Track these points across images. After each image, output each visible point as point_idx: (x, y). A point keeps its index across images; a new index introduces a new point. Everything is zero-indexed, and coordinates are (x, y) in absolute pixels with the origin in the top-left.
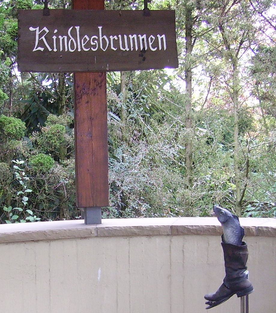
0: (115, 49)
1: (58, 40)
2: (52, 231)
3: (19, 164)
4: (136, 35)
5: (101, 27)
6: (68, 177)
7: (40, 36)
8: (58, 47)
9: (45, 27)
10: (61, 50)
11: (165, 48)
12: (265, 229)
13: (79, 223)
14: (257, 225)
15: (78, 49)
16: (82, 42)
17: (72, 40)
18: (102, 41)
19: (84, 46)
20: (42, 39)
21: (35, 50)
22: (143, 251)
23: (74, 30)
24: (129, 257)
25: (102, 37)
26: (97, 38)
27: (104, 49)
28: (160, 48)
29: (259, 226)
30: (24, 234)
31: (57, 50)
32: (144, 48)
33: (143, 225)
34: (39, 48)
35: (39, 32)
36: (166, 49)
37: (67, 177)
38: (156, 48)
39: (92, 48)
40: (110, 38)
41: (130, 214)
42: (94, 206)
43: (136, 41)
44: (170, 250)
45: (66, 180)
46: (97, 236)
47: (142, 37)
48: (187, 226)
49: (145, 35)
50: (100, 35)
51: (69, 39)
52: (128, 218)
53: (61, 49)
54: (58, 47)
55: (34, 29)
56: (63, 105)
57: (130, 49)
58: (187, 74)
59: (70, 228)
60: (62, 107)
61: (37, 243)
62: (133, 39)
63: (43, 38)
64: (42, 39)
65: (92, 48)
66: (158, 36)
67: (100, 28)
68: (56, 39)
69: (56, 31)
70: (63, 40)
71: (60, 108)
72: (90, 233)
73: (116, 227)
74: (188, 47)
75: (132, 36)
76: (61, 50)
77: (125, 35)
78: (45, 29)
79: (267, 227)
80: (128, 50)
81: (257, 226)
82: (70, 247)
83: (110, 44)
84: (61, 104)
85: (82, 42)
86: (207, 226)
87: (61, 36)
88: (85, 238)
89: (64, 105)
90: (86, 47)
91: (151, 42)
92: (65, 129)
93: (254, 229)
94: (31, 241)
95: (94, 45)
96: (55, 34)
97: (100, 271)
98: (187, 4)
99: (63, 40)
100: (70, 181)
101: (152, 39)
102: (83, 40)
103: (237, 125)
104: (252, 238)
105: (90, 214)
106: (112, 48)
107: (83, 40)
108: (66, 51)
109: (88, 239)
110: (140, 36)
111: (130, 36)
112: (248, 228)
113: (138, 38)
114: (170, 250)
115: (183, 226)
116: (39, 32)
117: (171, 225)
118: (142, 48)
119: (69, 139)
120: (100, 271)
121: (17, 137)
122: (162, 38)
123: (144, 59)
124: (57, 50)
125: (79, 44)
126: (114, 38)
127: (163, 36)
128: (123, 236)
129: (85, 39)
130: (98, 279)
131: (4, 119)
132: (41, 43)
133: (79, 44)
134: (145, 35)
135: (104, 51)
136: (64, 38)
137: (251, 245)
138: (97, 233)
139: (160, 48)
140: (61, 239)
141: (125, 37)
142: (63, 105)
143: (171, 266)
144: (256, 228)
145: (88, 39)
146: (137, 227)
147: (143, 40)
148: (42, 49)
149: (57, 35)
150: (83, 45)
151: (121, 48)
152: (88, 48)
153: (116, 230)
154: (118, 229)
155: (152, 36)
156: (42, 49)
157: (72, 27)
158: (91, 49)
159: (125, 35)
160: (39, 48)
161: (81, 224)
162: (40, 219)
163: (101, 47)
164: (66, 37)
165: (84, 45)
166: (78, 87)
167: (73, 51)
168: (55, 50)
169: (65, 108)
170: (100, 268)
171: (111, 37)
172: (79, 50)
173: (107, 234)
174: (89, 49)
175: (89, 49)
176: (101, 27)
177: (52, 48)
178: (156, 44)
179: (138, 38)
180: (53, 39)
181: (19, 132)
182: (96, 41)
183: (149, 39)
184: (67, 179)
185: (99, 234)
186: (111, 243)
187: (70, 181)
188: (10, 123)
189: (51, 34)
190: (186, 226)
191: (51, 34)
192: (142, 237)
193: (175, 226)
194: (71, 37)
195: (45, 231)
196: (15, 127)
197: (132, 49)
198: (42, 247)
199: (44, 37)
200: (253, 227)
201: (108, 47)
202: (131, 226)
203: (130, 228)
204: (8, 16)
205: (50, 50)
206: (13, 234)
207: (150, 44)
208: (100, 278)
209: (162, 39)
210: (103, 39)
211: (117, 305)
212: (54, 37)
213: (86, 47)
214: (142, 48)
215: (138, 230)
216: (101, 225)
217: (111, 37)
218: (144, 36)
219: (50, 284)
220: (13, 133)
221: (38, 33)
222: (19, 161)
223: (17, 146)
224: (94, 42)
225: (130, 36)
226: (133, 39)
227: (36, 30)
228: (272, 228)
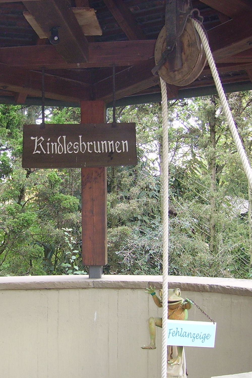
0: (91, 152)
1: (50, 146)
2: (60, 282)
3: (68, 231)
4: (106, 141)
5: (81, 136)
6: (110, 242)
7: (38, 143)
8: (50, 151)
9: (42, 137)
10: (52, 153)
11: (127, 151)
12: (215, 287)
13: (84, 277)
14: (210, 283)
15: (64, 152)
16: (68, 147)
17: (60, 146)
18: (82, 146)
19: (69, 150)
20: (39, 145)
21: (34, 153)
22: (128, 300)
23: (62, 138)
24: (118, 305)
25: (82, 143)
26: (78, 144)
27: (83, 152)
28: (124, 151)
29: (211, 284)
30: (38, 283)
31: (49, 153)
32: (112, 150)
33: (128, 281)
34: (37, 152)
35: (37, 140)
36: (128, 151)
37: (109, 242)
38: (121, 151)
39: (74, 151)
40: (87, 144)
41: (158, 272)
42: (94, 265)
43: (106, 146)
44: (148, 300)
45: (109, 244)
46: (94, 288)
47: (111, 143)
48: (160, 282)
49: (113, 141)
50: (81, 142)
51: (58, 145)
52: (157, 275)
53: (53, 152)
54: (50, 151)
55: (34, 138)
56: (114, 185)
57: (102, 152)
58: (212, 162)
59: (74, 281)
60: (114, 187)
61: (49, 290)
62: (104, 144)
63: (40, 144)
64: (39, 145)
65: (74, 151)
66: (122, 141)
67: (80, 137)
68: (49, 145)
69: (49, 139)
70: (54, 145)
71: (112, 188)
72: (88, 285)
73: (107, 281)
74: (212, 141)
75: (103, 142)
76: (52, 153)
77: (98, 142)
78: (42, 138)
79: (217, 285)
80: (100, 152)
81: (210, 284)
82: (73, 294)
83: (87, 148)
84: (113, 185)
85: (68, 147)
86: (175, 283)
87: (53, 143)
88: (85, 288)
89: (115, 186)
90: (70, 150)
91: (117, 146)
92: (110, 204)
93: (208, 286)
94: (44, 289)
95: (76, 149)
96: (49, 142)
97: (96, 313)
98: (206, 108)
99: (54, 145)
100: (112, 245)
101: (118, 144)
102: (68, 146)
103: (250, 202)
104: (207, 293)
105: (92, 270)
106: (89, 151)
107: (68, 146)
108: (56, 153)
109: (88, 289)
110: (109, 142)
111: (102, 142)
112: (204, 286)
113: (108, 144)
114: (148, 300)
115: (157, 282)
116: (37, 140)
117: (148, 281)
118: (110, 151)
119: (113, 213)
120: (96, 313)
121: (71, 211)
122: (125, 143)
123: (112, 159)
124: (49, 153)
125: (65, 148)
126: (90, 144)
127: (126, 142)
128: (113, 288)
129: (70, 145)
130: (94, 320)
131: (61, 197)
132: (39, 148)
133: (65, 148)
134: (113, 141)
135: (83, 153)
136: (55, 144)
137: (206, 299)
138: (94, 285)
139: (124, 151)
140: (66, 288)
141: (98, 143)
142: (114, 185)
143: (148, 313)
144: (209, 286)
145: (72, 145)
146: (124, 281)
147: (111, 144)
148: (39, 152)
149: (50, 142)
150: (68, 149)
151: (95, 151)
152: (71, 152)
153: (108, 283)
154: (109, 283)
155: (117, 142)
156: (39, 152)
157: (61, 136)
158: (73, 152)
159: (98, 142)
160: (37, 152)
161: (85, 278)
162: (86, 273)
163: (81, 150)
164: (56, 144)
165: (69, 149)
166: (84, 176)
167: (60, 153)
168: (48, 153)
169: (116, 188)
170: (96, 312)
171: (88, 143)
172: (65, 153)
173: (101, 286)
174: (72, 152)
175: (72, 152)
176: (81, 136)
177: (46, 151)
178: (120, 148)
179: (108, 144)
180: (47, 145)
181: (73, 207)
182: (77, 146)
183: (116, 144)
184: (109, 243)
185: (95, 286)
186: (104, 293)
187: (112, 245)
188: (66, 200)
189: (46, 141)
190: (160, 282)
191: (46, 141)
192: (128, 290)
193: (151, 282)
194: (60, 143)
195: (54, 282)
196: (69, 203)
197: (103, 152)
198: (52, 294)
199: (41, 144)
200: (207, 284)
201: (86, 150)
202: (119, 280)
203: (118, 282)
204: (70, 120)
205: (45, 153)
206: (30, 283)
207: (117, 148)
208: (96, 320)
209: (125, 144)
210: (83, 145)
211: (108, 340)
212: (48, 144)
213: (70, 150)
214: (110, 151)
215: (124, 284)
216: (100, 279)
217: (88, 143)
218: (112, 142)
219: (58, 321)
220: (68, 207)
221: (36, 141)
222: (68, 229)
223: (71, 217)
224: (76, 147)
225: (102, 142)
226: (104, 144)
227: (35, 139)
228: (220, 286)
